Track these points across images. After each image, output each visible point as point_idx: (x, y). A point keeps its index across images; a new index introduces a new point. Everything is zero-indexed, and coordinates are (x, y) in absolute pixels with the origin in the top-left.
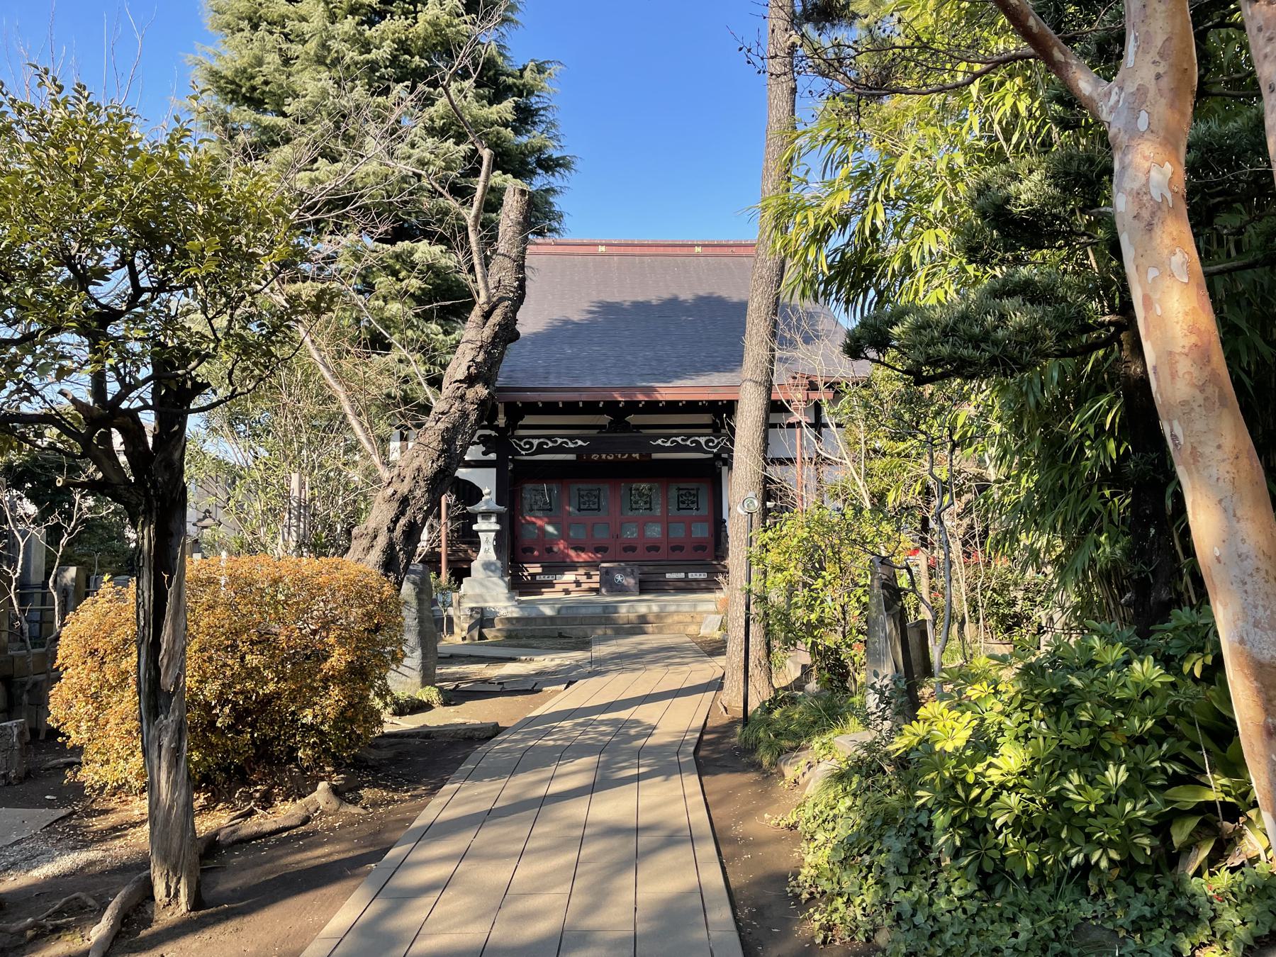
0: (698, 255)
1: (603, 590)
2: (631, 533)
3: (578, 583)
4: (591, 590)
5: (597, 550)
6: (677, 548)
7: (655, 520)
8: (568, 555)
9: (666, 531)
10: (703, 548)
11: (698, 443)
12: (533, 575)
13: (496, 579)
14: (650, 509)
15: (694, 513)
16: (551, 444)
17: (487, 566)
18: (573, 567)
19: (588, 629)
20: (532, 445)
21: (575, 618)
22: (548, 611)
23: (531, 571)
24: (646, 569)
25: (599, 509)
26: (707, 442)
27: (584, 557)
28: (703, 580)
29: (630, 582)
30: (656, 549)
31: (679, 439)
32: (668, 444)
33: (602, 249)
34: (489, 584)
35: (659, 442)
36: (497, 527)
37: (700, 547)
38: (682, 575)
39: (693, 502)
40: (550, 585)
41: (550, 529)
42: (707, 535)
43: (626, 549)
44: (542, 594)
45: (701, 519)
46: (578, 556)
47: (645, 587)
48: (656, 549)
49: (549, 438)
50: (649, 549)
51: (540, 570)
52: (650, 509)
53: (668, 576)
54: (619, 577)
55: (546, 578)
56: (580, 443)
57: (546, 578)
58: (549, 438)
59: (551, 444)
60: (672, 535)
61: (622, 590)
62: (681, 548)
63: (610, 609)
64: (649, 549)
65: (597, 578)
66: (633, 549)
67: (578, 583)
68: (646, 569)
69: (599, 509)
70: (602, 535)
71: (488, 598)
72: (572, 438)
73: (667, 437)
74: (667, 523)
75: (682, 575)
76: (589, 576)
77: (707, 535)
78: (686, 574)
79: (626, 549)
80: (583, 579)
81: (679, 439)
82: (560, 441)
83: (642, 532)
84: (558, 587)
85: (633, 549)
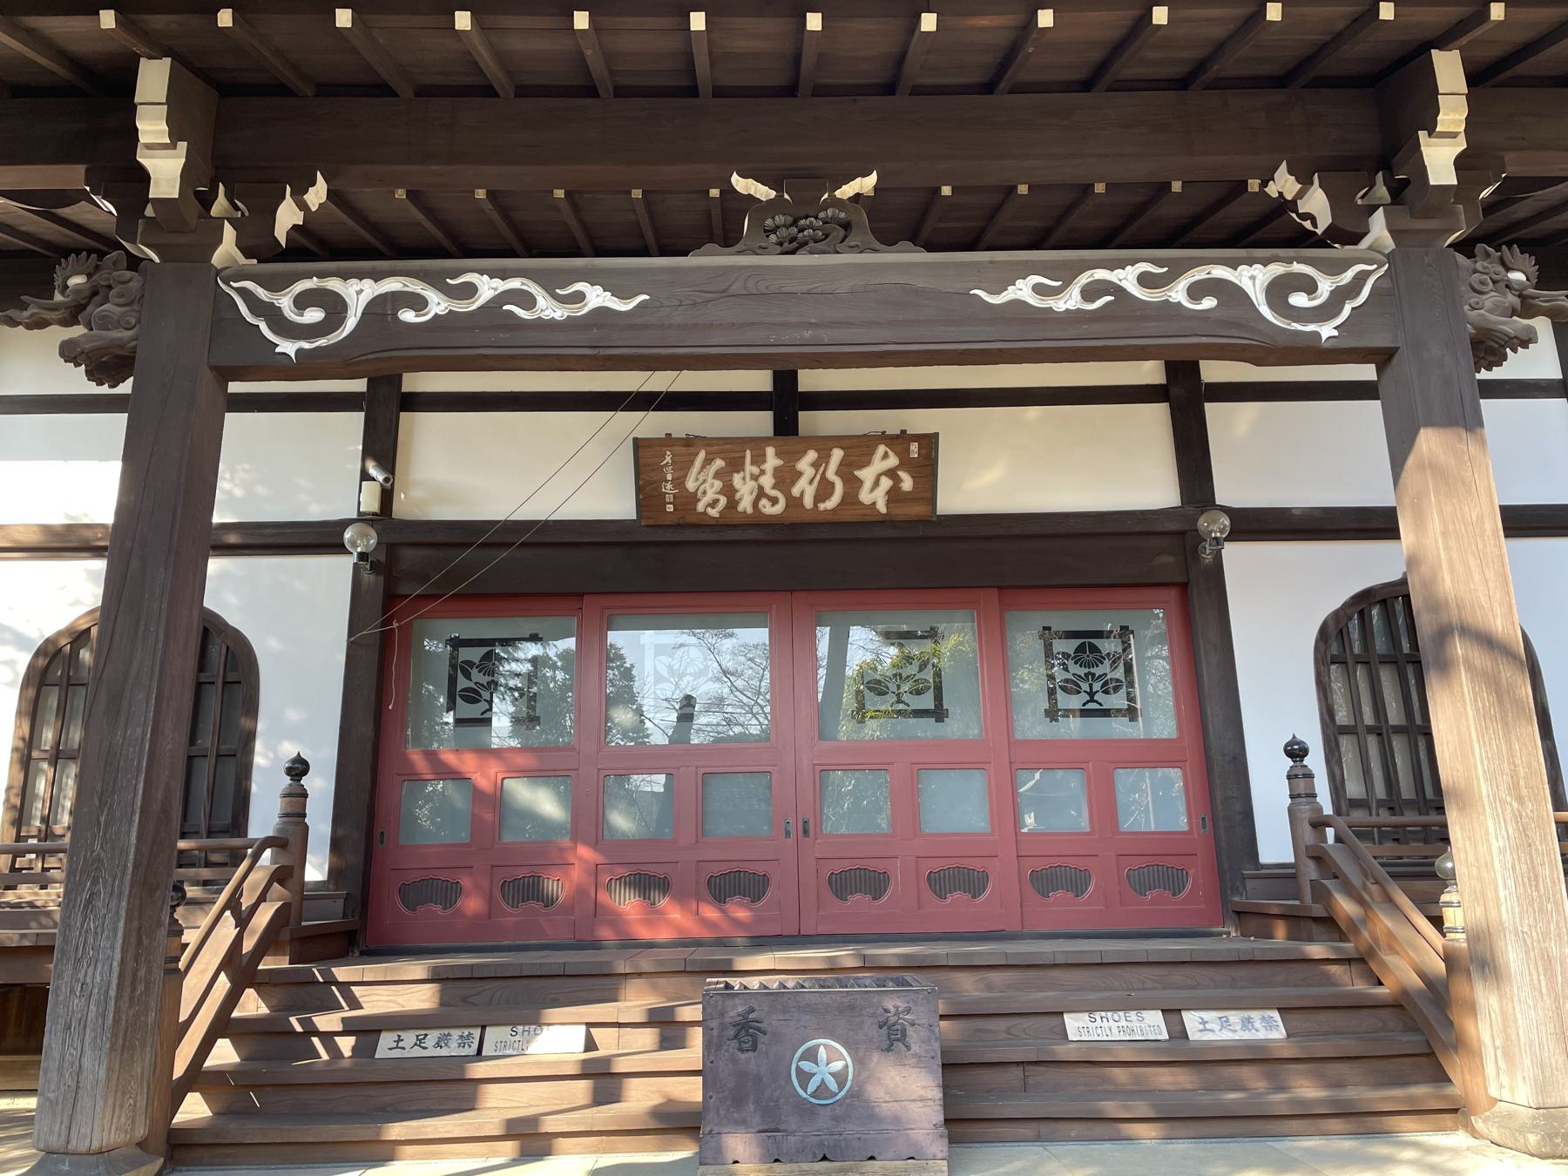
3: (603, 1080)
5: (728, 885)
7: (958, 758)
9: (1007, 806)
10: (1174, 881)
11: (1230, 293)
12: (367, 1030)
14: (939, 713)
15: (1119, 728)
18: (596, 983)
20: (335, 307)
23: (375, 1003)
24: (969, 987)
26: (1278, 291)
27: (676, 918)
28: (1257, 1057)
37: (1155, 864)
38: (1152, 1024)
39: (1109, 687)
40: (449, 1089)
42: (1182, 823)
43: (841, 885)
45: (1150, 755)
51: (421, 998)
52: (939, 713)
53: (1078, 1026)
54: (831, 1059)
65: (693, 1053)
67: (603, 1080)
68: (969, 987)
75: (1152, 1024)
76: (668, 1029)
77: (1182, 823)
79: (841, 885)
80: (632, 1047)
84: (500, 1104)
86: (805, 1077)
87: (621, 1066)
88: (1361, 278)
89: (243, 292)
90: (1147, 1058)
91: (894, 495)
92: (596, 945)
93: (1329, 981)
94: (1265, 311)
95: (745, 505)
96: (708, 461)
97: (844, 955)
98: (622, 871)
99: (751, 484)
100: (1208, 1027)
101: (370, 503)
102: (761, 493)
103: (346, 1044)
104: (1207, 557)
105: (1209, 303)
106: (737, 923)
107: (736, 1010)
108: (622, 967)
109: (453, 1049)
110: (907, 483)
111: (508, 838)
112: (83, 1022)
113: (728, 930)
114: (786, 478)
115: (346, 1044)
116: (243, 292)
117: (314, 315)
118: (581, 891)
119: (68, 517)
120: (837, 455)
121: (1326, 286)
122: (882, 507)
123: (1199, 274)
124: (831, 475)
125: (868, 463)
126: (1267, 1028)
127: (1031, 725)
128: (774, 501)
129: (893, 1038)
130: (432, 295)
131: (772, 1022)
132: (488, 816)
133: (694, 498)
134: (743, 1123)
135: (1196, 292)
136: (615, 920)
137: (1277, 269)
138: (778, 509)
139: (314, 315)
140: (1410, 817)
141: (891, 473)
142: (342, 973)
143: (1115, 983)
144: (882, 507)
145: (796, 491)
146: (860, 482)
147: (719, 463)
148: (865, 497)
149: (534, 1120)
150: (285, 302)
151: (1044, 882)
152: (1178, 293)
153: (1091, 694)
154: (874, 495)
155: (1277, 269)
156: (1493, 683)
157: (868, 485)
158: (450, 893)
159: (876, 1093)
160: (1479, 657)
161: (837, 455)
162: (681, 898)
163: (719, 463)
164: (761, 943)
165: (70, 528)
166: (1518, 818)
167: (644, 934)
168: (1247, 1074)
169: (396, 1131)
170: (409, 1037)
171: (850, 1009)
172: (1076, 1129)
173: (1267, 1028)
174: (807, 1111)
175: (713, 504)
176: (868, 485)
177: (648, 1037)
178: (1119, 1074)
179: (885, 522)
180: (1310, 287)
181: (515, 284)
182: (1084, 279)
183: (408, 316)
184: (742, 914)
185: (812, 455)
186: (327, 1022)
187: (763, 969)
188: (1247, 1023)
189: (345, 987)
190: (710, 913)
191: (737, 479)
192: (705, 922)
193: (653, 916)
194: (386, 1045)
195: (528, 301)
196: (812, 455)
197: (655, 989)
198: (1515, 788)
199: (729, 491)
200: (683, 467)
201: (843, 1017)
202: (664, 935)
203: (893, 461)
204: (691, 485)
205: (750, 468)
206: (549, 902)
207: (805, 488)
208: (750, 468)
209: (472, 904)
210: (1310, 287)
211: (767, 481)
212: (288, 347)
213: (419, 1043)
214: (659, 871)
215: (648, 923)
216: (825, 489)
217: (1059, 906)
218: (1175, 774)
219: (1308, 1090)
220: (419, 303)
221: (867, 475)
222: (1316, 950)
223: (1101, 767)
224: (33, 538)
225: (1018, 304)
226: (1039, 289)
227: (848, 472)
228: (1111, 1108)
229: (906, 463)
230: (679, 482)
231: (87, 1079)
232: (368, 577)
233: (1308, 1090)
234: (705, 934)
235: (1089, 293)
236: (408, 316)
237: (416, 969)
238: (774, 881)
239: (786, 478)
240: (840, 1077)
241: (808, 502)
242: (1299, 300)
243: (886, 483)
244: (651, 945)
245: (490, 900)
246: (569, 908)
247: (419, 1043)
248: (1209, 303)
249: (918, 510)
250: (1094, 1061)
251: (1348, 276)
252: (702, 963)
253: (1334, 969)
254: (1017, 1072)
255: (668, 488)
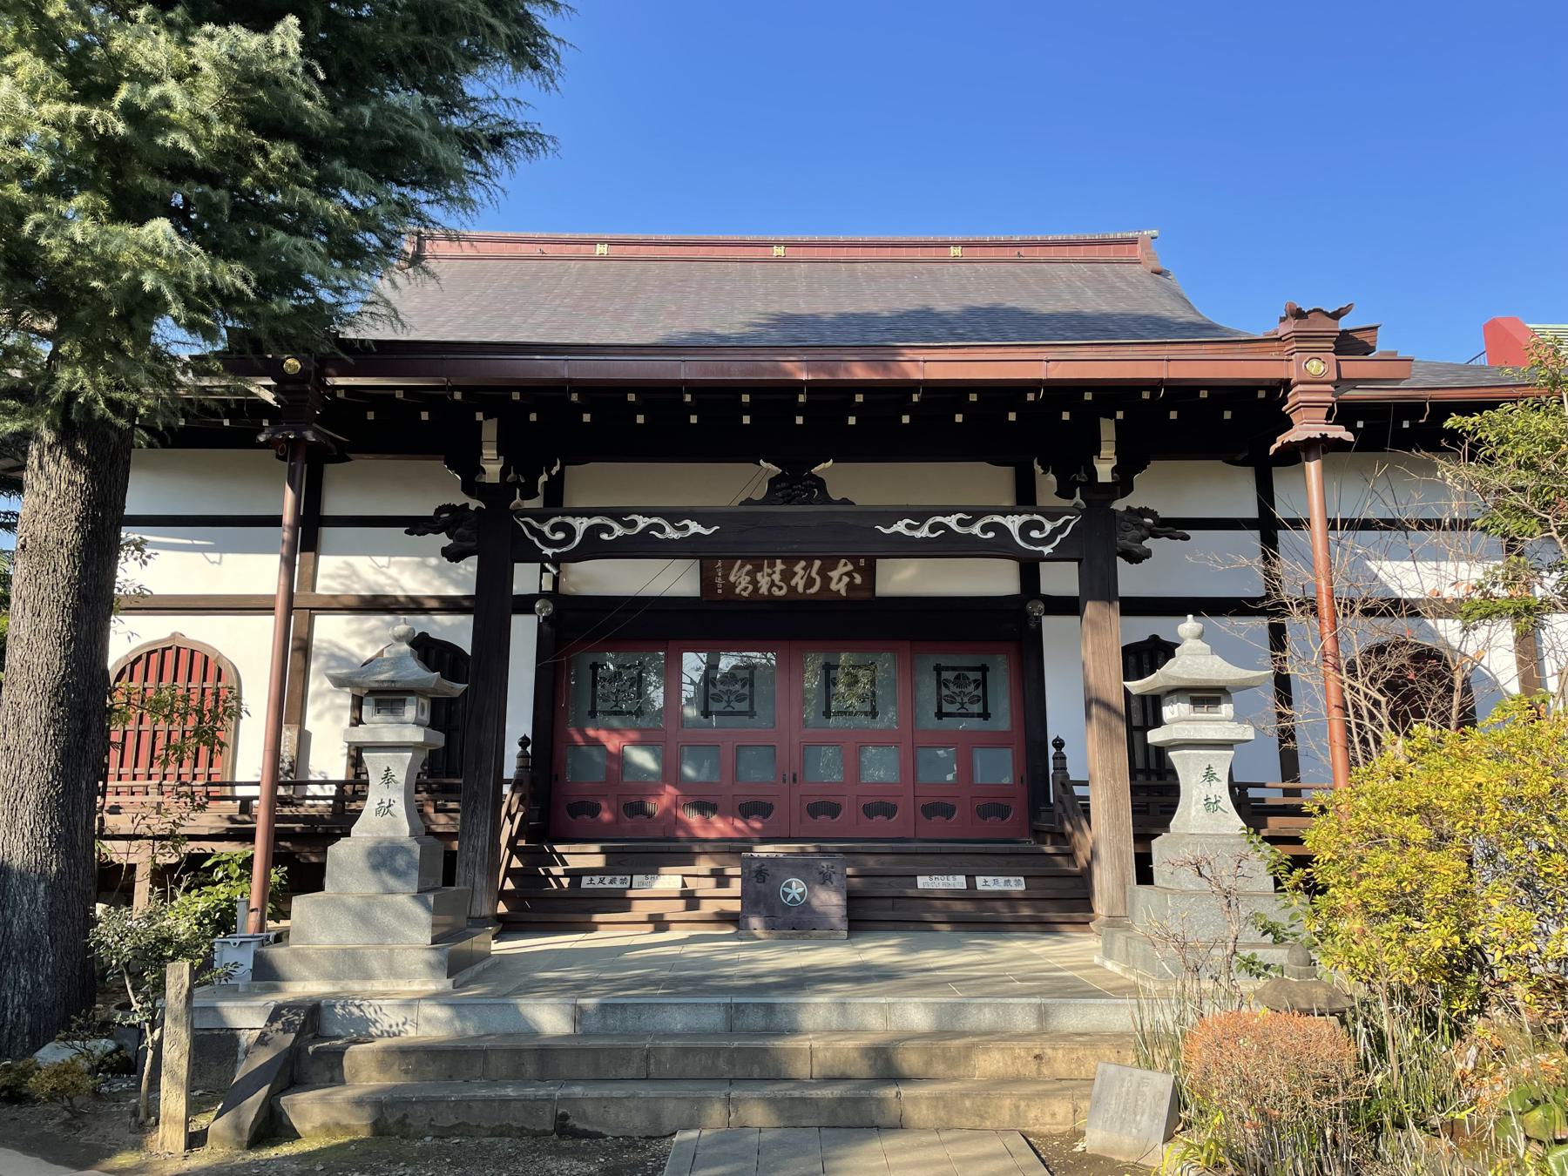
0: (955, 261)
1: (755, 922)
2: (827, 770)
3: (691, 899)
4: (724, 918)
5: (746, 811)
6: (937, 809)
8: (678, 823)
9: (911, 768)
10: (1002, 811)
11: (1001, 530)
12: (575, 875)
13: (404, 901)
16: (619, 531)
17: (383, 858)
18: (682, 854)
19: (671, 1101)
20: (570, 531)
21: (621, 1055)
22: (549, 1018)
23: (575, 862)
24: (871, 863)
25: (751, 713)
26: (1025, 529)
27: (720, 827)
28: (1004, 897)
29: (830, 901)
30: (888, 810)
31: (951, 521)
32: (923, 532)
33: (778, 251)
34: (386, 919)
35: (900, 527)
36: (416, 735)
37: (993, 806)
38: (959, 882)
40: (619, 902)
41: (643, 759)
43: (815, 810)
44: (591, 927)
45: (996, 741)
46: (707, 824)
47: (862, 918)
48: (888, 810)
49: (618, 514)
50: (870, 810)
51: (598, 861)
53: (923, 882)
54: (797, 887)
55: (607, 883)
56: (694, 528)
57: (607, 883)
58: (618, 514)
59: (619, 531)
60: (923, 777)
61: (796, 923)
62: (946, 810)
63: (761, 1009)
64: (870, 810)
65: (736, 887)
66: (833, 810)
67: (691, 899)
68: (871, 863)
69: (751, 713)
70: (758, 776)
71: (375, 965)
72: (674, 516)
73: (920, 515)
74: (913, 745)
75: (959, 882)
76: (721, 879)
78: (970, 878)
79: (815, 810)
80: (706, 887)
81: (951, 521)
82: (643, 523)
83: (854, 767)
84: (641, 910)
85: (833, 810)
86: (786, 895)
87: (698, 894)
88: (1067, 523)
89: (526, 523)
90: (955, 896)
91: (851, 586)
92: (676, 840)
93: (1056, 864)
94: (1018, 540)
95: (764, 590)
96: (742, 566)
97: (810, 847)
98: (690, 800)
99: (767, 579)
100: (985, 884)
101: (548, 586)
102: (773, 584)
103: (565, 882)
104: (1033, 625)
105: (991, 535)
106: (753, 829)
107: (755, 866)
108: (697, 849)
109: (618, 885)
110: (858, 580)
111: (626, 779)
112: (474, 863)
113: (749, 834)
114: (787, 575)
115: (565, 882)
116: (526, 523)
117: (560, 536)
118: (667, 811)
119: (370, 588)
120: (817, 563)
121: (1049, 527)
122: (843, 593)
123: (987, 520)
124: (814, 574)
125: (835, 568)
126: (1016, 885)
127: (929, 721)
128: (780, 588)
129: (825, 880)
130: (616, 526)
131: (772, 870)
132: (615, 767)
133: (734, 586)
134: (759, 914)
135: (985, 529)
136: (686, 827)
137: (1025, 518)
138: (783, 592)
139: (560, 536)
140: (1154, 780)
141: (848, 574)
142: (559, 848)
143: (942, 863)
144: (843, 593)
145: (793, 583)
146: (831, 579)
147: (749, 567)
148: (833, 587)
149: (662, 915)
150: (546, 529)
151: (930, 810)
152: (976, 530)
153: (962, 704)
154: (839, 585)
155: (1025, 518)
156: (1106, 726)
157: (835, 580)
158: (595, 810)
159: (815, 902)
160: (1103, 714)
161: (817, 563)
162: (723, 815)
163: (749, 567)
164: (765, 841)
165: (375, 597)
166: (1113, 788)
167: (701, 834)
168: (998, 904)
169: (598, 918)
170: (596, 879)
171: (807, 866)
172: (912, 926)
173: (1016, 885)
174: (787, 908)
175: (745, 589)
176: (835, 580)
177: (712, 881)
178: (937, 903)
179: (845, 601)
180: (1041, 527)
181: (655, 520)
182: (931, 521)
183: (604, 536)
184: (757, 825)
185: (803, 563)
186: (557, 870)
187: (764, 850)
188: (996, 882)
189: (560, 855)
190: (739, 824)
191: (759, 576)
192: (736, 829)
193: (707, 824)
194: (585, 882)
195: (661, 529)
196: (803, 563)
197: (713, 860)
198: (1113, 774)
199: (754, 582)
200: (727, 570)
201: (800, 866)
202: (713, 835)
203: (850, 567)
204: (732, 579)
205: (767, 570)
206: (650, 816)
207: (799, 581)
208: (767, 570)
209: (606, 816)
210: (1041, 527)
211: (776, 577)
212: (548, 552)
213: (601, 881)
214: (711, 800)
215: (705, 828)
216: (810, 582)
217: (937, 826)
218: (1007, 754)
219: (1026, 912)
220: (610, 530)
221: (835, 574)
222: (1049, 849)
223: (965, 747)
224: (354, 603)
225: (897, 533)
226: (908, 526)
227: (823, 573)
228: (928, 917)
229: (857, 569)
230: (726, 577)
231: (478, 887)
232: (546, 628)
233: (1026, 912)
234: (736, 835)
235: (933, 529)
236: (604, 536)
237: (595, 848)
238: (776, 805)
239: (787, 575)
240: (802, 895)
241: (800, 589)
242: (1035, 534)
243: (846, 579)
244: (706, 840)
245: (617, 815)
246: (659, 819)
247: (601, 881)
248: (991, 535)
249: (866, 595)
250: (928, 898)
251: (1061, 521)
252: (734, 848)
253: (1058, 858)
254: (890, 902)
255: (719, 580)
